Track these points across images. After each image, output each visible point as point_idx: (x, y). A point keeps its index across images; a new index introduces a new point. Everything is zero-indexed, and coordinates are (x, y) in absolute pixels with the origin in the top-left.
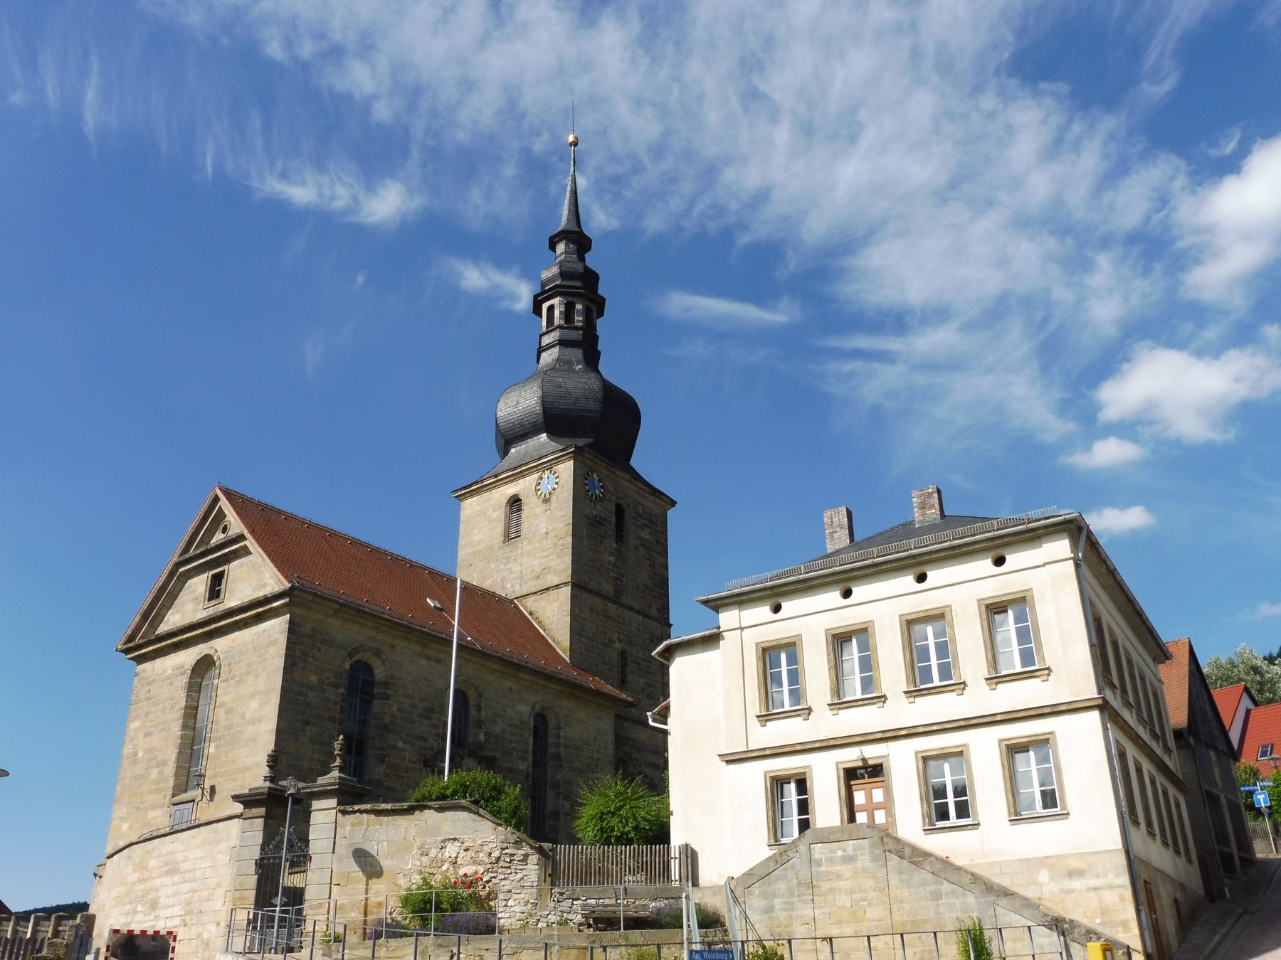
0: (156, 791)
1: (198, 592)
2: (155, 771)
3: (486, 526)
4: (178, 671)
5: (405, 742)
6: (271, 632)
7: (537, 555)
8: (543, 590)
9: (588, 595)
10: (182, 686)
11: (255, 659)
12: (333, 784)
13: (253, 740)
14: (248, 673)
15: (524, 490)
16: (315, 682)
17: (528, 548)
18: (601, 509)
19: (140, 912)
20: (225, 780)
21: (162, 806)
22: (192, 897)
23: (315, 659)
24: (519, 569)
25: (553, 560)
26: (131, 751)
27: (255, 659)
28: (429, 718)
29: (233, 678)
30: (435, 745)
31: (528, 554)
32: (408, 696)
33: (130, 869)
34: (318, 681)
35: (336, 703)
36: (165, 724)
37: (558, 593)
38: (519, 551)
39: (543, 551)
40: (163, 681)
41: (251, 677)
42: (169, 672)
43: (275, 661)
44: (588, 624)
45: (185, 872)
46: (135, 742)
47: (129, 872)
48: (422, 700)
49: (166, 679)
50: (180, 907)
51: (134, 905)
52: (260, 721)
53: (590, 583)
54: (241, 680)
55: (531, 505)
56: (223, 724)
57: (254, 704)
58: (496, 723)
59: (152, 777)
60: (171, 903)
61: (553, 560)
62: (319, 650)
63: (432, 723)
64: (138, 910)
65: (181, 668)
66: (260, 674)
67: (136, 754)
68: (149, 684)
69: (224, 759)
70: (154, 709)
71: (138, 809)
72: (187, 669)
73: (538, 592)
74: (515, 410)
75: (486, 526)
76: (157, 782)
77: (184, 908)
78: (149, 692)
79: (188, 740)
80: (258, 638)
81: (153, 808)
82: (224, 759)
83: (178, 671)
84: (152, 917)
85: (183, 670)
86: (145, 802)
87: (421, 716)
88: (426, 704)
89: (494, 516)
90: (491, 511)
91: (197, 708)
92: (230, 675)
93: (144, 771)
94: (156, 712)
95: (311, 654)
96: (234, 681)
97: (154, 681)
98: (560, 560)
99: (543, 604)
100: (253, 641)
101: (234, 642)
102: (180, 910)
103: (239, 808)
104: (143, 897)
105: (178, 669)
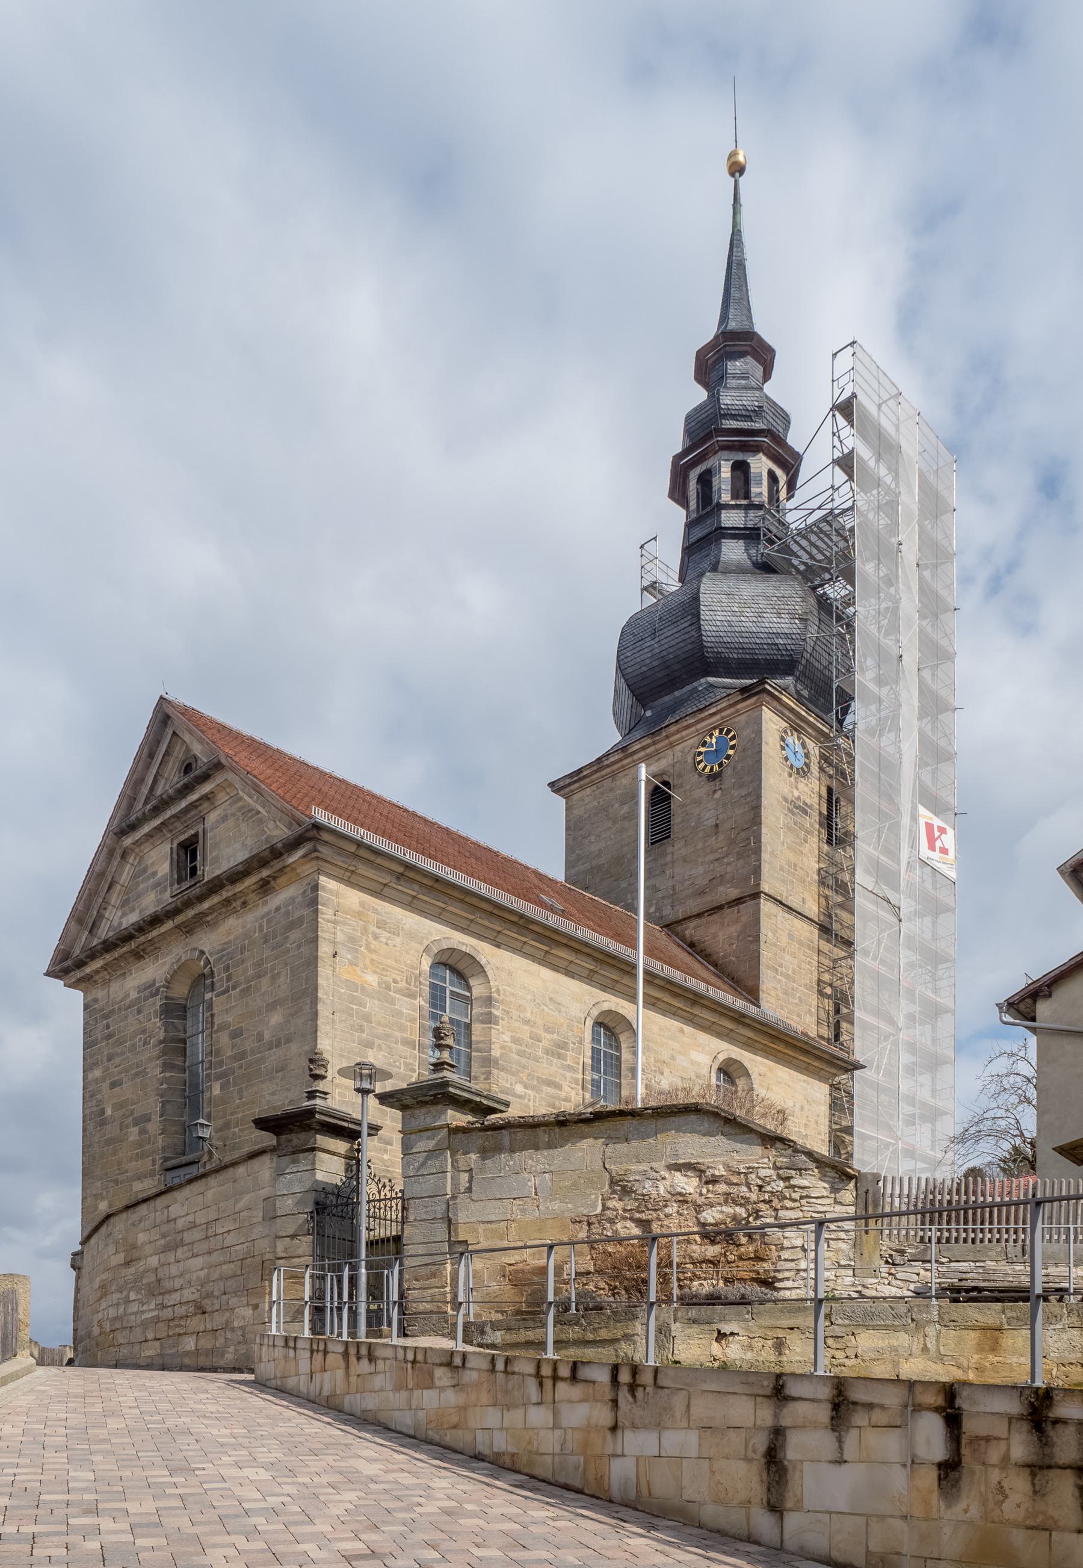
0: (141, 1156)
1: (160, 874)
2: (133, 1133)
3: (609, 829)
4: (147, 993)
5: (526, 1087)
6: (290, 908)
7: (700, 860)
8: (711, 910)
9: (787, 915)
10: (156, 1012)
11: (267, 953)
12: (447, 1069)
13: (282, 1068)
14: (259, 976)
15: (673, 766)
16: (375, 984)
17: (683, 851)
18: (806, 789)
19: (134, 1300)
20: (244, 1130)
21: (152, 1174)
22: (209, 1274)
23: (370, 951)
24: (670, 884)
25: (729, 864)
26: (95, 1109)
27: (267, 953)
28: (559, 1056)
29: (234, 988)
30: (573, 1094)
31: (685, 861)
32: (527, 1022)
33: (112, 1249)
34: (379, 984)
35: (413, 1020)
36: (138, 1067)
37: (739, 912)
38: (669, 858)
39: (711, 852)
40: (126, 1009)
41: (265, 982)
42: (134, 995)
43: (302, 949)
44: (787, 957)
45: (193, 1243)
46: (99, 1097)
47: (110, 1253)
48: (547, 1030)
49: (129, 1007)
50: (193, 1290)
51: (125, 1293)
52: (289, 1040)
53: (790, 898)
54: (249, 988)
55: (688, 787)
56: (229, 1053)
57: (276, 1018)
58: (662, 1073)
59: (131, 1139)
60: (177, 1286)
61: (729, 864)
62: (376, 938)
63: (566, 1063)
64: (131, 1299)
65: (149, 987)
66: (279, 973)
67: (102, 1112)
68: (105, 1017)
69: (237, 1101)
70: (118, 1050)
71: (116, 1182)
72: (160, 987)
73: (703, 913)
74: (653, 642)
75: (609, 829)
76: (140, 1145)
77: (198, 1290)
78: (108, 1027)
79: (176, 1085)
80: (269, 921)
81: (139, 1178)
82: (237, 1101)
83: (147, 993)
84: (152, 1306)
85: (154, 989)
86: (127, 1172)
87: (547, 1052)
88: (555, 1036)
89: (622, 812)
90: (616, 806)
91: (184, 1041)
92: (230, 983)
93: (118, 1132)
94: (123, 1053)
95: (364, 942)
96: (238, 990)
97: (113, 1011)
98: (741, 863)
99: (712, 930)
100: (261, 926)
101: (229, 935)
102: (193, 1293)
103: (268, 1139)
104: (135, 1281)
105: (145, 989)
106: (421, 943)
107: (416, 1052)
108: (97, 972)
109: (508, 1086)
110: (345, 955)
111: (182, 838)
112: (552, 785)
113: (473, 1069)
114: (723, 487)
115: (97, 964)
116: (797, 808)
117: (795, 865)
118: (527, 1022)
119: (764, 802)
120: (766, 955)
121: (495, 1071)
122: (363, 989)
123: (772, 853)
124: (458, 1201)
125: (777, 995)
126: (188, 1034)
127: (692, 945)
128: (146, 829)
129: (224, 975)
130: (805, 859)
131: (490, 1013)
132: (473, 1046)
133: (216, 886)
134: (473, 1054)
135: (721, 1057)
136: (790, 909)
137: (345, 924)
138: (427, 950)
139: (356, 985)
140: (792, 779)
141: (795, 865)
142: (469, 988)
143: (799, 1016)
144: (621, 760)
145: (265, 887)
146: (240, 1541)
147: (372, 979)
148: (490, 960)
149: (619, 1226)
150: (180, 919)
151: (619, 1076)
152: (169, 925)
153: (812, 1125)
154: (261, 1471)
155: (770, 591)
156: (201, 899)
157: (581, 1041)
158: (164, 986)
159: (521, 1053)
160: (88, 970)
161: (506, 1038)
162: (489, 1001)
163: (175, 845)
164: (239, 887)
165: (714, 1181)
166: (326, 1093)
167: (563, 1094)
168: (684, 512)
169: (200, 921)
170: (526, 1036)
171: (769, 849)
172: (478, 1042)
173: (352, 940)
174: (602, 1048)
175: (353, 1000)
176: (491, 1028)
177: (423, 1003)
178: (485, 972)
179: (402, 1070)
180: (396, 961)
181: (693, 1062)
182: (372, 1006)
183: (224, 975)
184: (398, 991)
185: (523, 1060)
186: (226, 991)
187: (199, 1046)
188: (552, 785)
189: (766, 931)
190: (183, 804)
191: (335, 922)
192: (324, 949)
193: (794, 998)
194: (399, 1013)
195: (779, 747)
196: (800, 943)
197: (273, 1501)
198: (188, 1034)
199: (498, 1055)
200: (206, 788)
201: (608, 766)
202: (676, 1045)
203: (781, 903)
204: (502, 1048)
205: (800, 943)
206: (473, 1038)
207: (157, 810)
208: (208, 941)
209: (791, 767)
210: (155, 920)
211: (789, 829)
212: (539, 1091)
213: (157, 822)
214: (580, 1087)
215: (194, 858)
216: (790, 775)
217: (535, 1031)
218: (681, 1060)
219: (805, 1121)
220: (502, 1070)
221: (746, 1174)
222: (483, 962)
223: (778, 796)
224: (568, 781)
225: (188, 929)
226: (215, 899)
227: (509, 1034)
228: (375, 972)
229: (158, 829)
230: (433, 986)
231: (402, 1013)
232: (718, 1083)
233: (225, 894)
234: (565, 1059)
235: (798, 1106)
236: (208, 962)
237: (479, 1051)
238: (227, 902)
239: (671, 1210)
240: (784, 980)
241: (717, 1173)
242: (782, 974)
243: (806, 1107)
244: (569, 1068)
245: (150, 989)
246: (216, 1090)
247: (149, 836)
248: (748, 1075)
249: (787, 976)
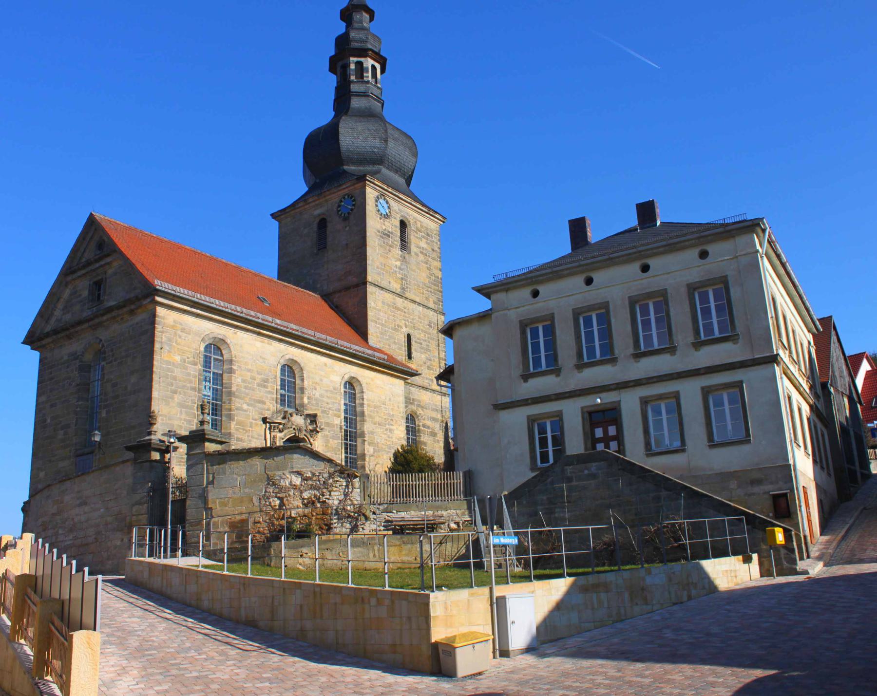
5: (248, 405)
9: (381, 292)
16: (179, 361)
18: (389, 224)
23: (178, 344)
28: (265, 387)
32: (249, 371)
34: (181, 361)
35: (195, 377)
42: (66, 358)
44: (382, 314)
48: (259, 374)
58: (316, 389)
62: (180, 337)
63: (268, 390)
67: (45, 421)
87: (259, 385)
88: (262, 376)
90: (302, 229)
91: (89, 385)
106: (200, 337)
107: (197, 393)
108: (48, 344)
109: (240, 406)
110: (166, 348)
111: (95, 280)
112: (272, 215)
113: (223, 398)
114: (351, 73)
115: (49, 340)
116: (384, 235)
117: (385, 265)
118: (249, 371)
119: (368, 234)
120: (371, 314)
121: (233, 399)
122: (173, 363)
123: (372, 260)
124: (209, 488)
125: (377, 335)
126: (91, 381)
127: (337, 307)
128: (79, 273)
129: (111, 353)
130: (389, 261)
131: (231, 368)
132: (224, 386)
133: (110, 310)
134: (224, 390)
135: (346, 377)
136: (382, 288)
137: (166, 332)
138: (203, 340)
139: (170, 362)
140: (382, 221)
141: (385, 265)
142: (222, 355)
143: (389, 345)
144: (304, 206)
145: (132, 312)
146: (136, 638)
147: (178, 358)
148: (232, 341)
149: (271, 500)
150: (91, 323)
151: (295, 393)
152: (86, 325)
153: (396, 408)
154: (137, 619)
155: (371, 127)
156: (103, 315)
157: (275, 377)
158: (81, 355)
159: (246, 388)
160: (44, 342)
161: (239, 380)
162: (231, 362)
163: (91, 283)
164: (121, 312)
165: (307, 479)
166: (156, 432)
167: (266, 407)
168: (335, 76)
169: (100, 325)
170: (248, 379)
171: (371, 259)
172: (226, 384)
173: (170, 340)
174: (286, 378)
175: (169, 370)
176: (232, 376)
177: (200, 367)
178: (229, 347)
179: (190, 404)
180: (189, 347)
181: (331, 381)
182: (178, 372)
183: (111, 353)
184: (189, 363)
185: (247, 391)
186: (111, 362)
187: (96, 388)
188: (272, 215)
189: (371, 303)
190: (97, 265)
191: (162, 332)
192: (157, 346)
193: (386, 336)
194: (189, 374)
195: (374, 205)
196: (388, 305)
197: (142, 628)
198: (91, 381)
199: (235, 390)
200: (108, 260)
201: (298, 208)
202: (323, 373)
203: (377, 286)
204: (237, 386)
205: (388, 305)
206: (224, 381)
207: (84, 267)
208: (104, 334)
209: (381, 214)
210: (80, 323)
211: (381, 246)
212: (254, 406)
213: (83, 272)
214: (275, 402)
215: (99, 290)
216: (381, 219)
217: (252, 374)
218: (325, 381)
219: (391, 407)
220: (237, 398)
221: (318, 476)
222: (229, 342)
223: (374, 230)
224: (279, 214)
225: (95, 327)
226: (109, 316)
227: (240, 378)
228: (179, 354)
229: (84, 275)
230: (206, 356)
231: (191, 374)
232: (346, 390)
233: (114, 314)
234: (267, 388)
235: (388, 399)
236: (103, 346)
237: (226, 388)
238: (114, 318)
239: (291, 493)
240: (381, 327)
241: (308, 476)
242: (379, 324)
243: (392, 399)
244: (270, 392)
245: (74, 356)
246: (104, 415)
247: (80, 277)
248: (361, 385)
249: (382, 325)
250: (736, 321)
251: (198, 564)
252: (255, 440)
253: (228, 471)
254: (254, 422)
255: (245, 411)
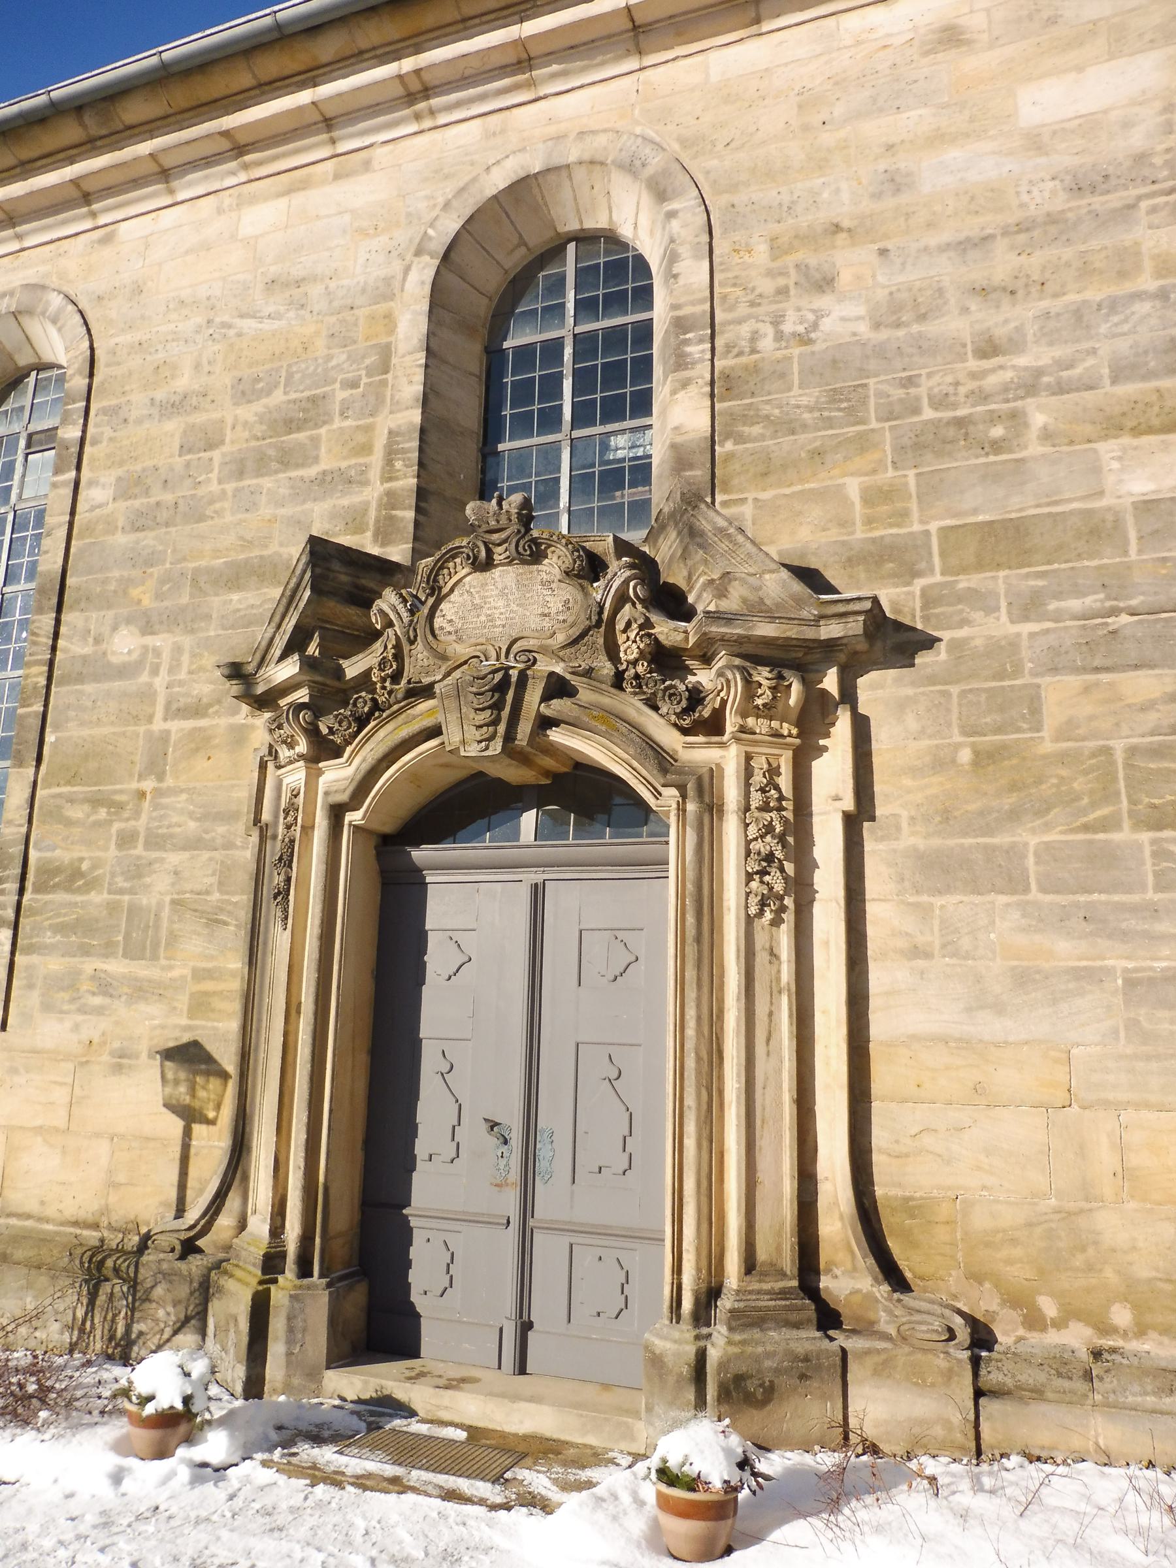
88: (278, 397)
109: (87, 650)
185: (148, 539)
250: (177, 1155)
251: (590, 461)
252: (174, 858)
253: (90, 1215)
254: (177, 727)
255: (125, 671)
